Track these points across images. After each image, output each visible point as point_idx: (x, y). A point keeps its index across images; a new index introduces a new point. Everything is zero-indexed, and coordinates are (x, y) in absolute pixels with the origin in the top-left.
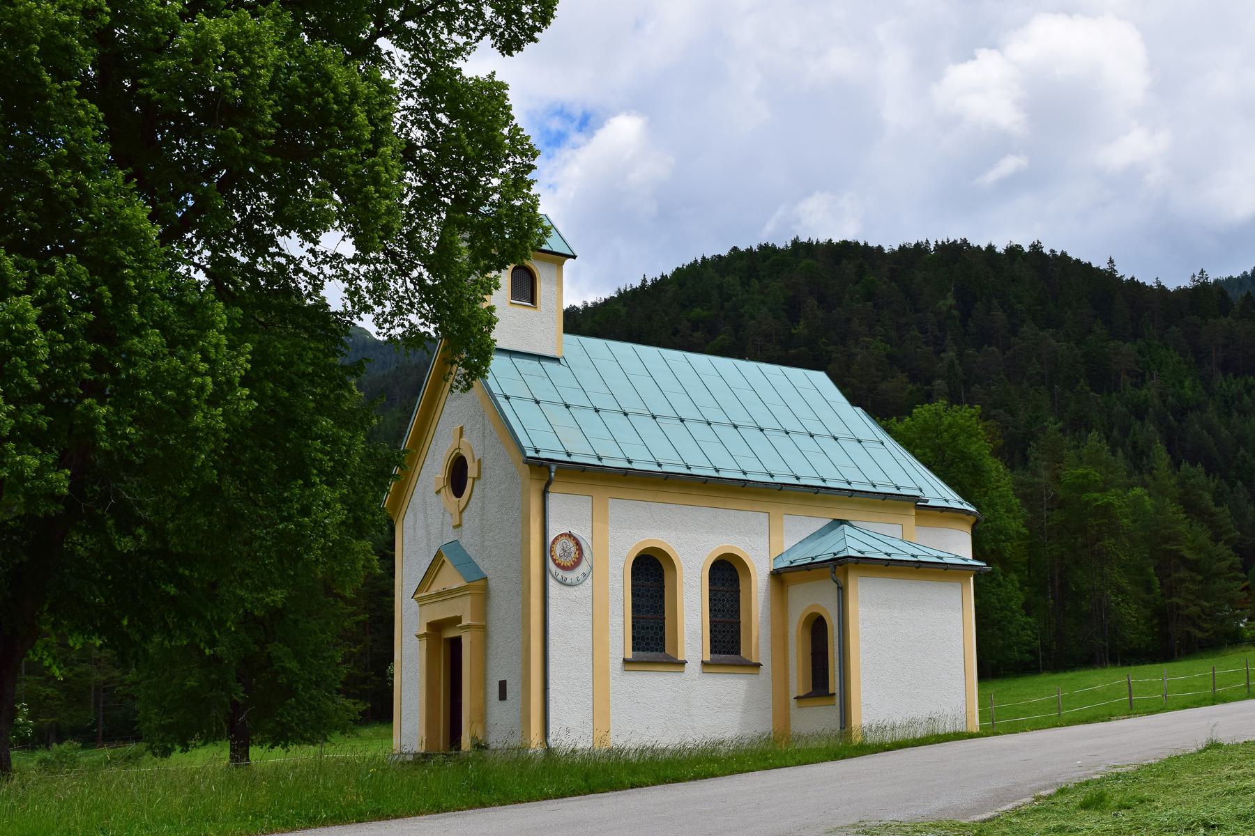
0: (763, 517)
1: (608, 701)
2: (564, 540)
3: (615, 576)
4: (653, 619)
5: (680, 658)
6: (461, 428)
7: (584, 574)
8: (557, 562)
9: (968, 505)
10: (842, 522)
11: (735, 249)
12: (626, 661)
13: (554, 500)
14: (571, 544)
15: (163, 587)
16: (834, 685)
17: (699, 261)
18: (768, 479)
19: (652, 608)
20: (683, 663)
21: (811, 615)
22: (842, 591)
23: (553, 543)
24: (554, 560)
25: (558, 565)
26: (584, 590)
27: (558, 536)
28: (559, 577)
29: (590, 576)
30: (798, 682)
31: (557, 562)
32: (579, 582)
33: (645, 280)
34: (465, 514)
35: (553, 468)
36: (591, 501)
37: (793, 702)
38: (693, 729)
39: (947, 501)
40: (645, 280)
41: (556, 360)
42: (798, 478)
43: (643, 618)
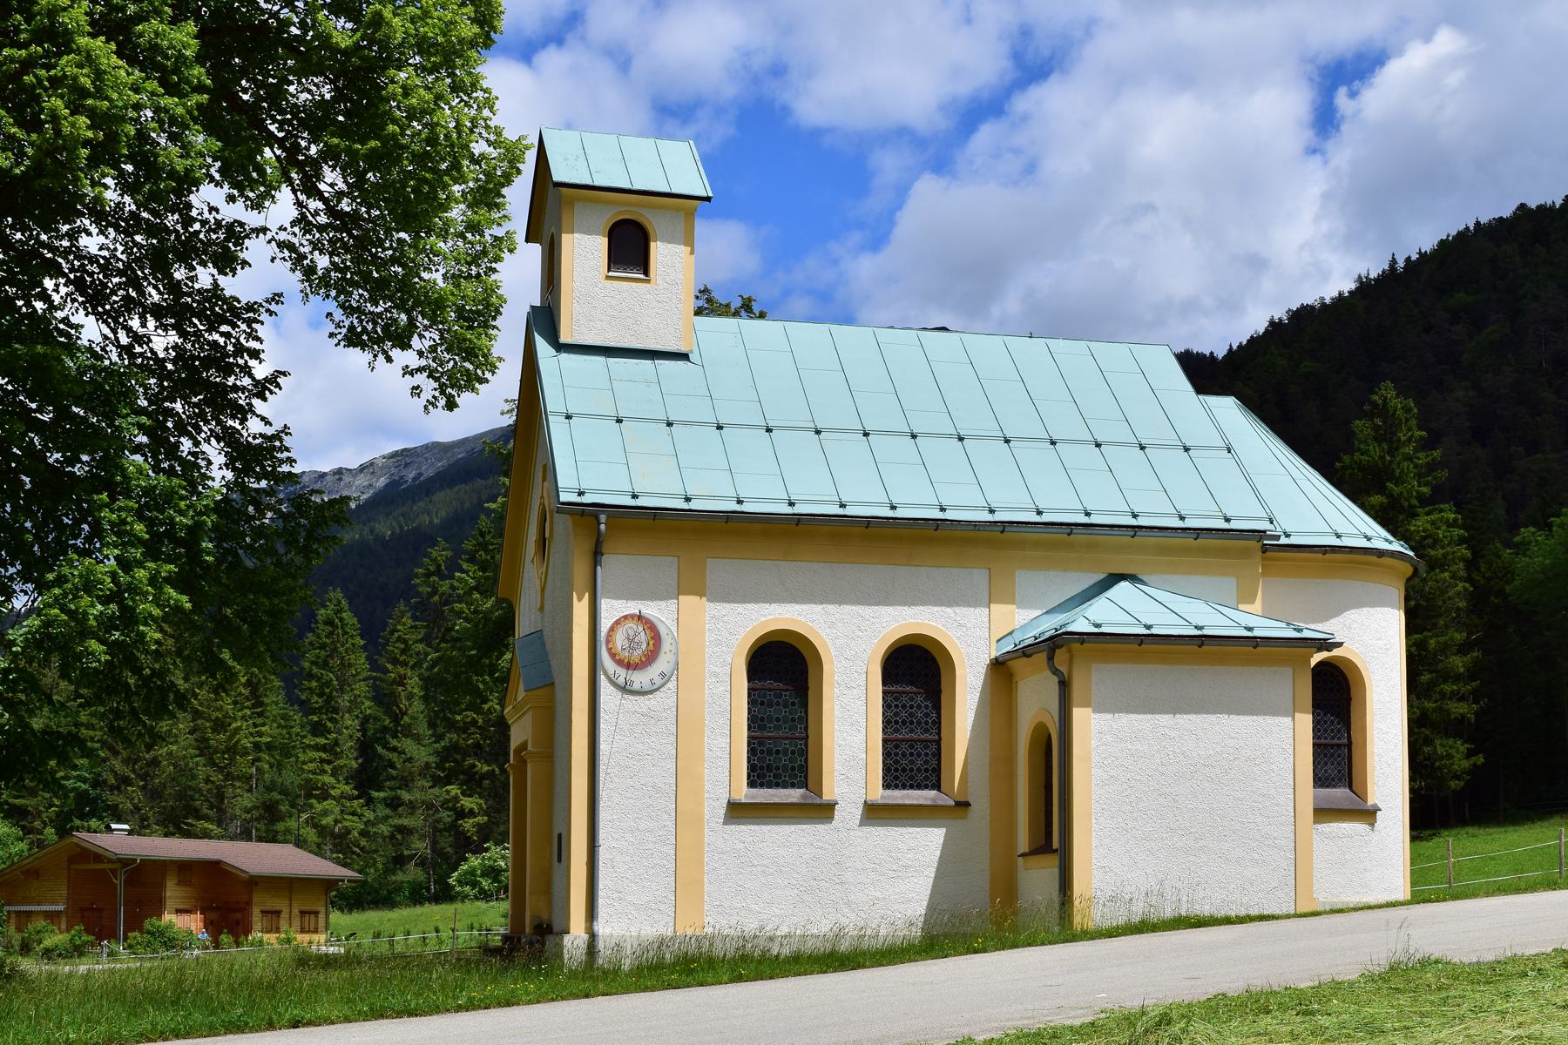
1: (701, 864)
2: (631, 626)
3: (716, 675)
4: (787, 738)
7: (663, 675)
8: (617, 658)
9: (1402, 546)
11: (1522, 206)
15: (1475, 654)
17: (1472, 228)
19: (785, 722)
23: (612, 629)
24: (613, 656)
25: (620, 662)
26: (662, 701)
27: (620, 619)
28: (621, 681)
29: (674, 677)
31: (617, 658)
32: (655, 687)
33: (1394, 261)
35: (603, 518)
36: (676, 564)
38: (848, 904)
39: (1369, 539)
40: (1394, 261)
41: (683, 356)
42: (1182, 518)
43: (769, 738)
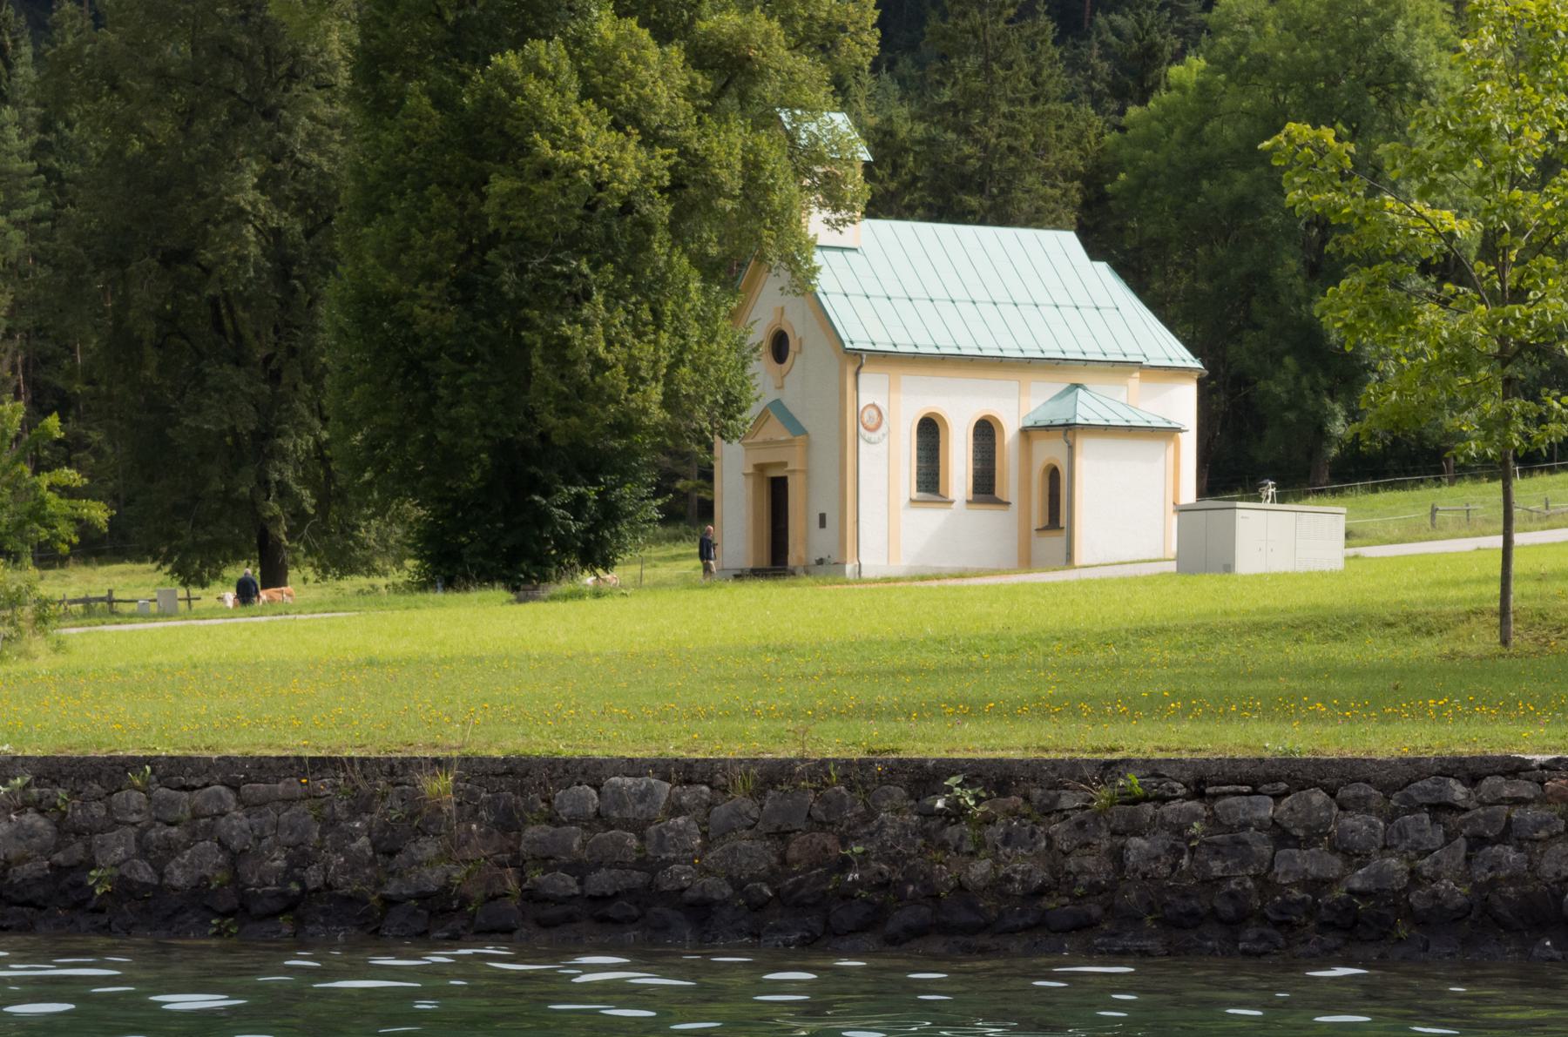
0: (1014, 385)
5: (951, 498)
6: (783, 309)
10: (1077, 386)
12: (912, 501)
13: (863, 377)
14: (874, 413)
16: (1063, 521)
18: (1020, 355)
20: (952, 502)
21: (1049, 465)
22: (1071, 448)
25: (866, 428)
26: (883, 447)
30: (1038, 516)
34: (787, 379)
37: (1034, 533)
41: (856, 250)
